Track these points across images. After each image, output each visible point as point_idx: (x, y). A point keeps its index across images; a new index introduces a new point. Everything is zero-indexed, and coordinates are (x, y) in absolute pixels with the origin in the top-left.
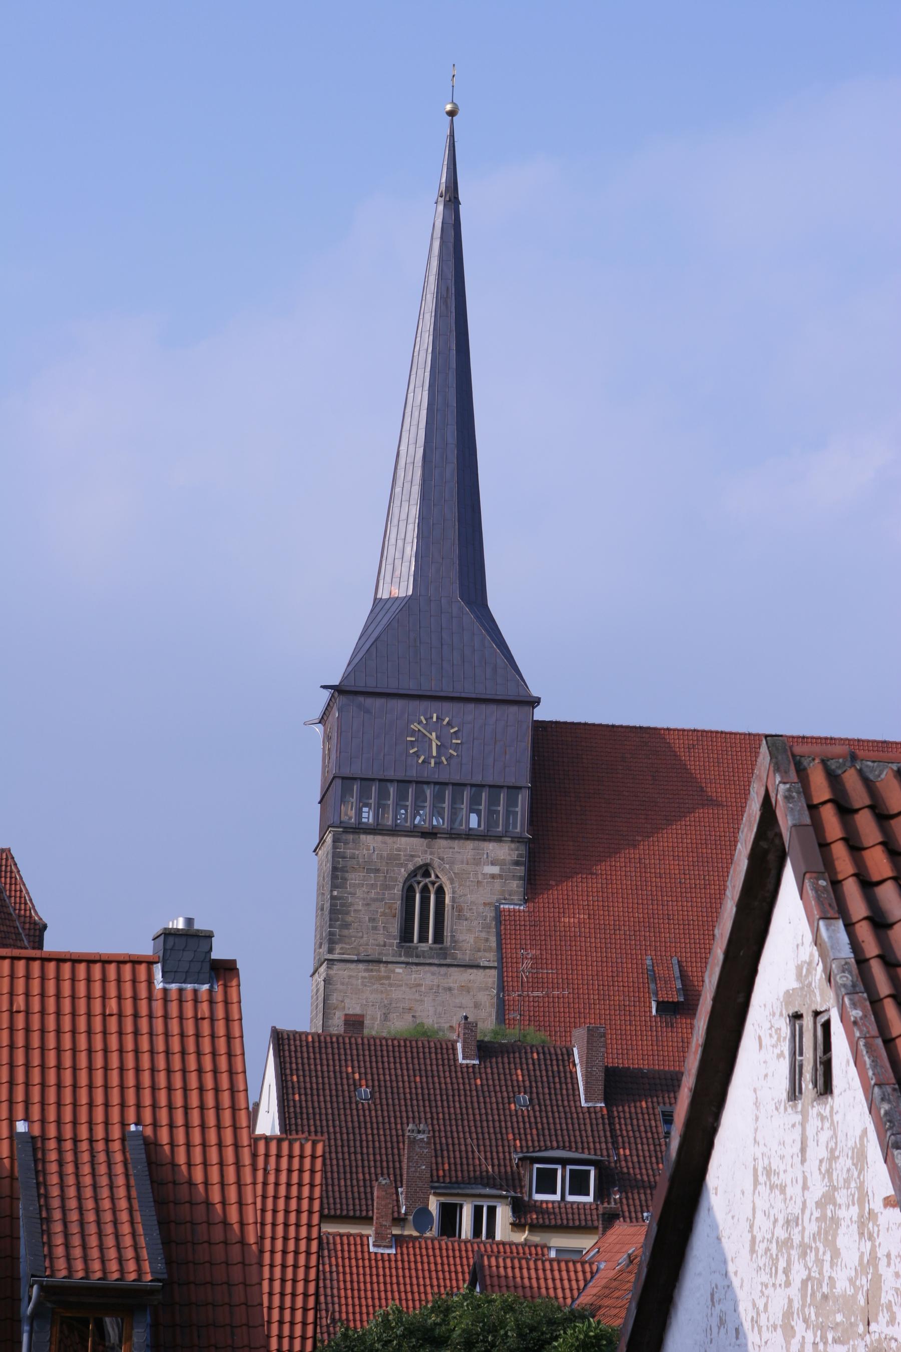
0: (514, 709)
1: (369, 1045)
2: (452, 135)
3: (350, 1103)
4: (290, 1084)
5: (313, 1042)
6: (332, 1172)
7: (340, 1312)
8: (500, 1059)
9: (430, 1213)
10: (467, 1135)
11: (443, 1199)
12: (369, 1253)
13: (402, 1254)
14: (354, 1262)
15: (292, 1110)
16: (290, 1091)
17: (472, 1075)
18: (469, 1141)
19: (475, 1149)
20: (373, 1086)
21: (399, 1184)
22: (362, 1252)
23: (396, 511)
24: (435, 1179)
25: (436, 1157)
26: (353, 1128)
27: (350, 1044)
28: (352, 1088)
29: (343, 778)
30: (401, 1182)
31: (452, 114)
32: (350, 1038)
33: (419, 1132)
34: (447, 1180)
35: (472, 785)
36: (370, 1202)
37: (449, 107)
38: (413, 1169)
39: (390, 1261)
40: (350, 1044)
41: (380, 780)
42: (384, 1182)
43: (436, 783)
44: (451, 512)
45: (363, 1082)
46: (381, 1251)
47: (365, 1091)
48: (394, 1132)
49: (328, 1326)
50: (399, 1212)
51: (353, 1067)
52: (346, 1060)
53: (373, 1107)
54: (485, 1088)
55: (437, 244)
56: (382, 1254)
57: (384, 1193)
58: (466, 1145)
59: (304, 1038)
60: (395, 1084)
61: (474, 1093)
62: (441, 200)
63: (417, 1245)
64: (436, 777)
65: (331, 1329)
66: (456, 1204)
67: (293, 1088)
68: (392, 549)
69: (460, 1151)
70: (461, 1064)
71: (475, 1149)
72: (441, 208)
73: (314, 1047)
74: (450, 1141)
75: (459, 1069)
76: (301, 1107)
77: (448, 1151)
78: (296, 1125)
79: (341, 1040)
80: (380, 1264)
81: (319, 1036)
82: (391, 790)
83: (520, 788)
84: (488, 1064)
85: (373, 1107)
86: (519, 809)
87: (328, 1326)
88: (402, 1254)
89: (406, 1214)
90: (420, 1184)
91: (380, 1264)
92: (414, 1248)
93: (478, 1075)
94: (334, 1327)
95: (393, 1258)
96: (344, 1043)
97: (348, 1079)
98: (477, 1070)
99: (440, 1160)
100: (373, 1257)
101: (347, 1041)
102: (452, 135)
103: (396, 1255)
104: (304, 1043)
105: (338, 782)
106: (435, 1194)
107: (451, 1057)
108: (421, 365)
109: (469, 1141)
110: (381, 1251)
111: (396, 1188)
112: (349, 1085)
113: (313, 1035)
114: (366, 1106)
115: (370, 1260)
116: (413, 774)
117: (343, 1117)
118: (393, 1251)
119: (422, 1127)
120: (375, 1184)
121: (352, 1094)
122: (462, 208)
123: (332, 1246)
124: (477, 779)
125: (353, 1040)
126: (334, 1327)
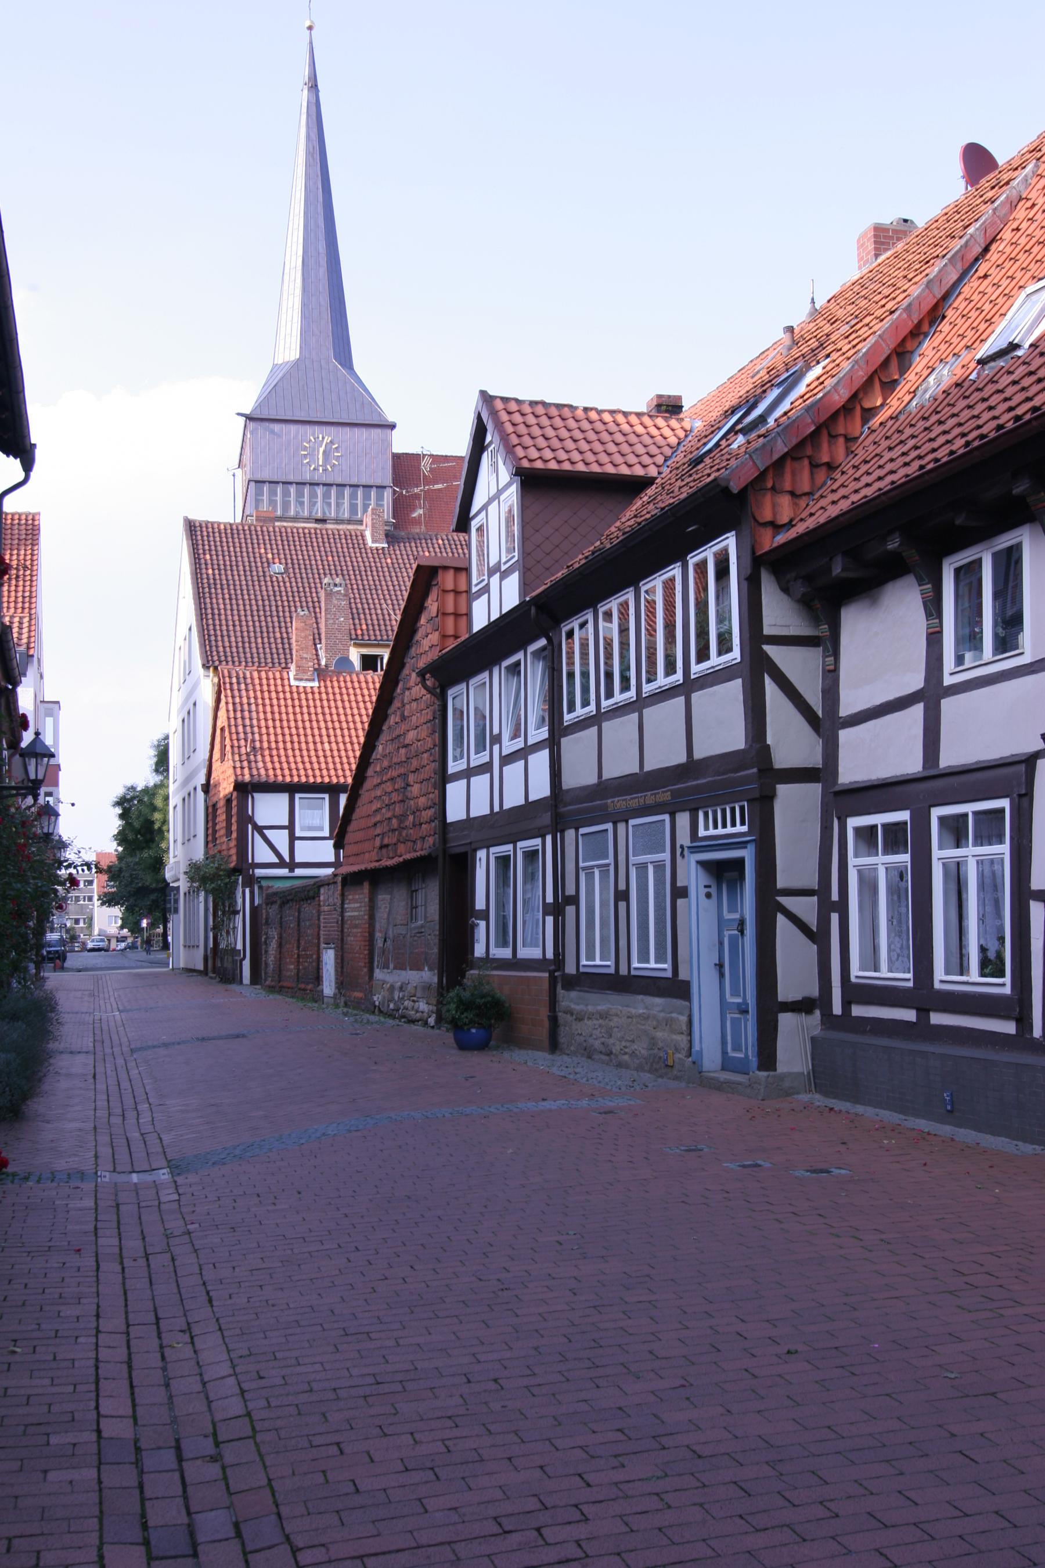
0: (379, 431)
1: (281, 532)
2: (311, 43)
3: (264, 576)
4: (203, 561)
5: (225, 529)
6: (248, 632)
7: (261, 741)
8: (407, 544)
9: (351, 663)
10: (383, 601)
11: (366, 651)
12: (290, 686)
13: (326, 687)
14: (274, 695)
15: (205, 581)
16: (203, 566)
17: (382, 556)
18: (384, 606)
19: (391, 612)
20: (286, 564)
21: (317, 641)
22: (283, 686)
23: (284, 304)
24: (354, 637)
25: (353, 619)
26: (268, 596)
27: (262, 531)
28: (266, 565)
29: (256, 482)
30: (320, 639)
31: (310, 28)
32: (261, 527)
33: (336, 585)
34: (366, 637)
35: (351, 486)
36: (288, 656)
37: (308, 24)
38: (331, 621)
39: (313, 693)
40: (262, 531)
41: (284, 483)
42: (302, 613)
43: (324, 485)
44: (324, 300)
45: (277, 560)
46: (302, 684)
47: (278, 568)
48: (309, 599)
49: (247, 754)
50: (319, 665)
51: (265, 549)
52: (258, 544)
53: (287, 579)
54: (396, 566)
55: (304, 117)
56: (304, 687)
57: (303, 624)
58: (382, 609)
59: (216, 526)
60: (307, 562)
61: (386, 569)
62: (306, 87)
63: (342, 679)
64: (324, 480)
65: (252, 757)
66: (377, 656)
67: (206, 564)
68: (283, 330)
69: (377, 615)
70: (371, 548)
71: (391, 612)
72: (306, 92)
73: (226, 534)
74: (366, 606)
75: (369, 551)
76: (214, 579)
77: (365, 614)
78: (210, 593)
79: (253, 528)
80: (303, 696)
81: (231, 525)
82: (292, 490)
83: (385, 487)
84: (397, 548)
85: (287, 579)
86: (385, 503)
87: (247, 754)
88: (326, 687)
89: (326, 666)
90: (339, 636)
91: (303, 696)
92: (339, 682)
93: (388, 556)
94: (255, 756)
95: (316, 690)
96: (256, 531)
97: (261, 558)
98: (386, 552)
99: (357, 621)
100: (294, 689)
101: (259, 529)
102: (311, 43)
103: (319, 687)
104: (216, 530)
105: (253, 484)
106: (356, 645)
107: (361, 542)
108: (297, 201)
109: (384, 606)
110: (302, 684)
111: (315, 645)
112: (262, 563)
113: (225, 524)
114: (280, 579)
115: (291, 693)
116: (307, 477)
117: (257, 588)
118: (316, 684)
119: (338, 580)
120: (294, 615)
121: (266, 569)
122: (321, 94)
123: (249, 681)
124: (354, 481)
125: (265, 529)
126: (255, 756)
